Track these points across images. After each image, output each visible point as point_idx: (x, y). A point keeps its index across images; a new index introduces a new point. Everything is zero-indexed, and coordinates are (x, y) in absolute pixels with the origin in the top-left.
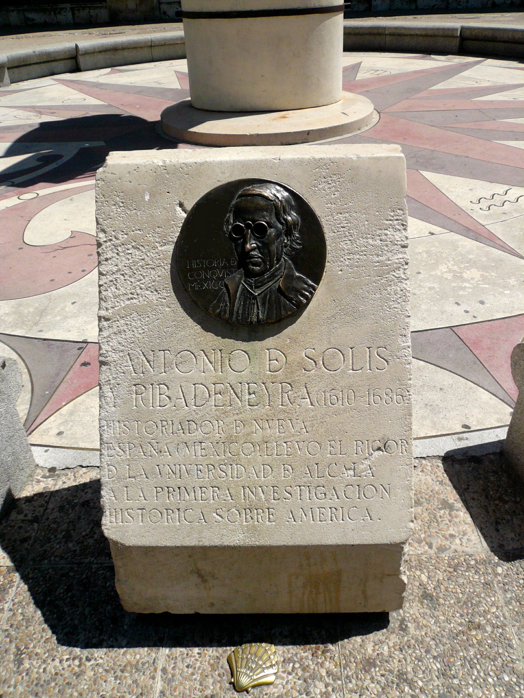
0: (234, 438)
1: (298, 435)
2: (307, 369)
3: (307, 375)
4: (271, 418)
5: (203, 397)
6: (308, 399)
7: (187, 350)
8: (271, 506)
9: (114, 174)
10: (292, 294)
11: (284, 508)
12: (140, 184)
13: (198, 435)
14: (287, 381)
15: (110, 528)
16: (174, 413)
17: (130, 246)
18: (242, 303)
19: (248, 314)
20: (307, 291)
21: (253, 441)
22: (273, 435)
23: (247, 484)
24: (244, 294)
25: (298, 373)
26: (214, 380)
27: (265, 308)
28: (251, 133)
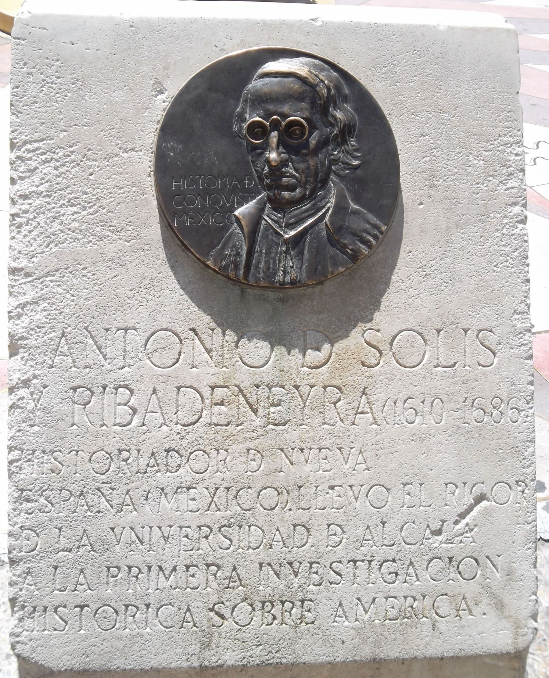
0: (246, 480)
1: (354, 475)
2: (367, 364)
3: (366, 374)
4: (308, 445)
5: (194, 409)
6: (370, 415)
7: (166, 329)
8: (309, 596)
9: (44, 29)
10: (345, 238)
11: (329, 598)
12: (88, 49)
13: (185, 475)
14: (335, 383)
15: (26, 640)
16: (143, 437)
17: (513, 165)
18: (264, 251)
19: (273, 269)
20: (369, 234)
21: (278, 484)
22: (312, 474)
23: (267, 560)
24: (267, 237)
25: (354, 371)
26: (214, 380)
27: (302, 259)
28: (378, 21)
